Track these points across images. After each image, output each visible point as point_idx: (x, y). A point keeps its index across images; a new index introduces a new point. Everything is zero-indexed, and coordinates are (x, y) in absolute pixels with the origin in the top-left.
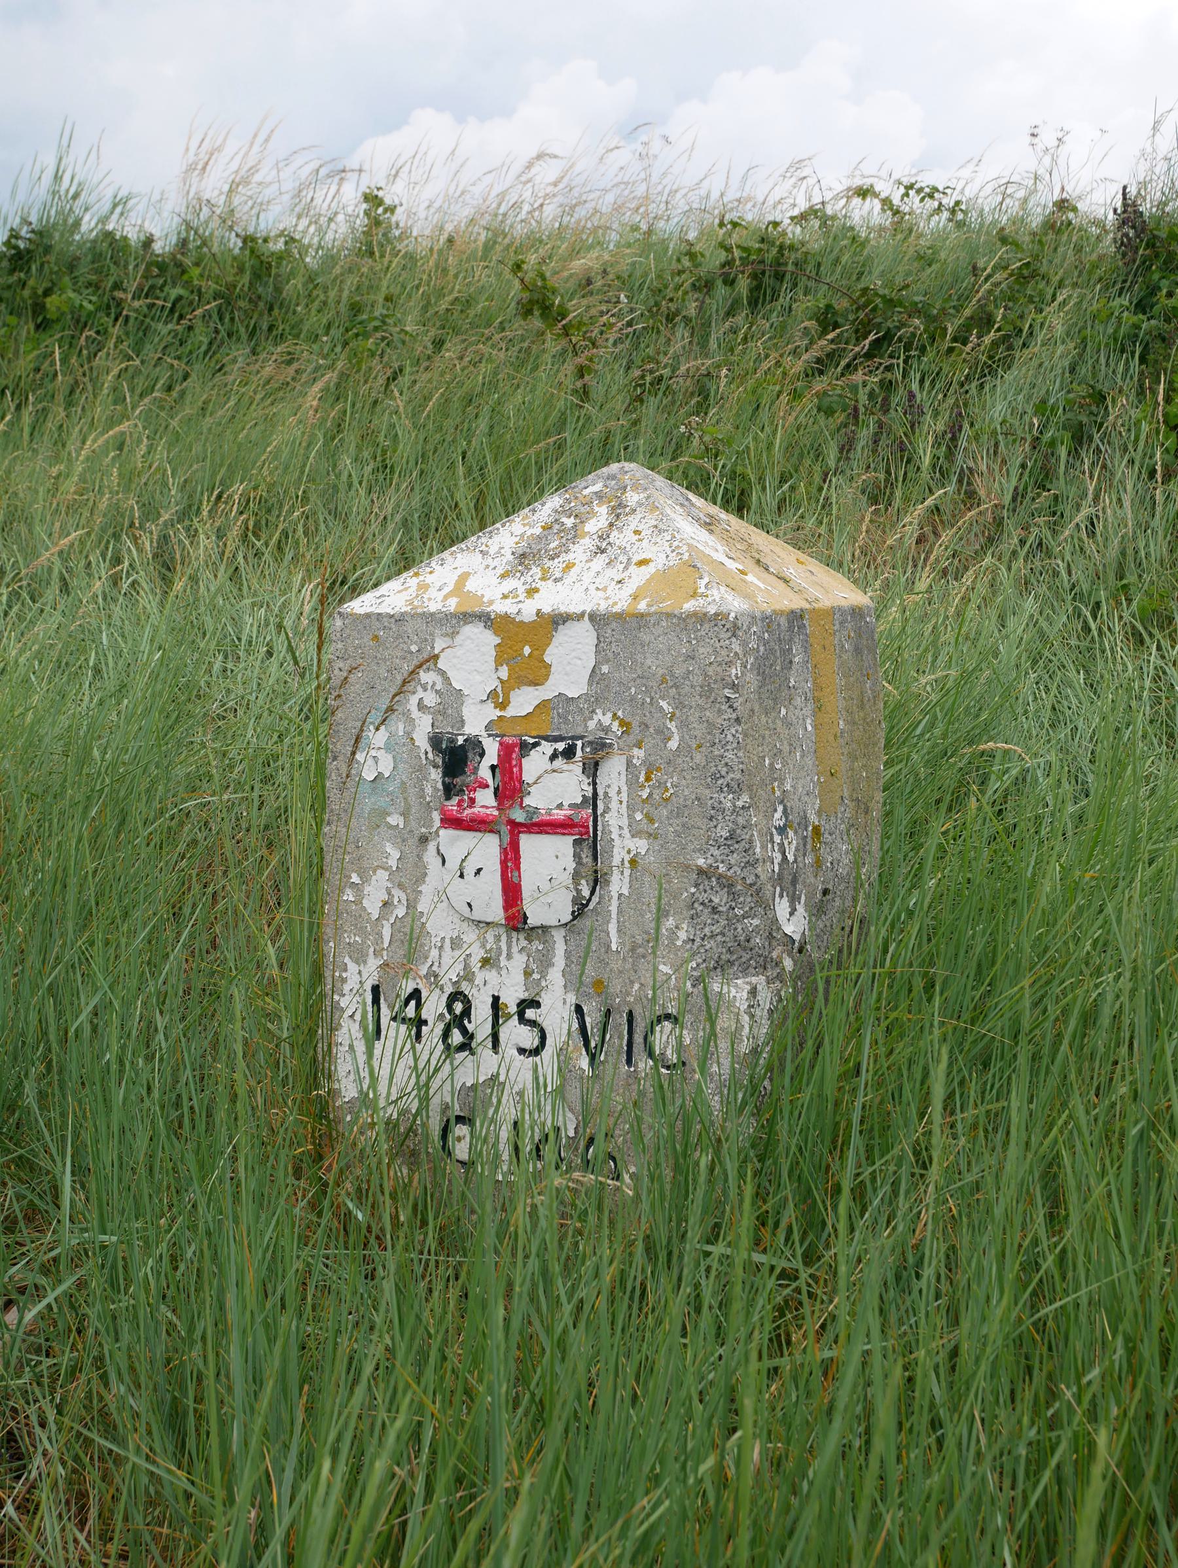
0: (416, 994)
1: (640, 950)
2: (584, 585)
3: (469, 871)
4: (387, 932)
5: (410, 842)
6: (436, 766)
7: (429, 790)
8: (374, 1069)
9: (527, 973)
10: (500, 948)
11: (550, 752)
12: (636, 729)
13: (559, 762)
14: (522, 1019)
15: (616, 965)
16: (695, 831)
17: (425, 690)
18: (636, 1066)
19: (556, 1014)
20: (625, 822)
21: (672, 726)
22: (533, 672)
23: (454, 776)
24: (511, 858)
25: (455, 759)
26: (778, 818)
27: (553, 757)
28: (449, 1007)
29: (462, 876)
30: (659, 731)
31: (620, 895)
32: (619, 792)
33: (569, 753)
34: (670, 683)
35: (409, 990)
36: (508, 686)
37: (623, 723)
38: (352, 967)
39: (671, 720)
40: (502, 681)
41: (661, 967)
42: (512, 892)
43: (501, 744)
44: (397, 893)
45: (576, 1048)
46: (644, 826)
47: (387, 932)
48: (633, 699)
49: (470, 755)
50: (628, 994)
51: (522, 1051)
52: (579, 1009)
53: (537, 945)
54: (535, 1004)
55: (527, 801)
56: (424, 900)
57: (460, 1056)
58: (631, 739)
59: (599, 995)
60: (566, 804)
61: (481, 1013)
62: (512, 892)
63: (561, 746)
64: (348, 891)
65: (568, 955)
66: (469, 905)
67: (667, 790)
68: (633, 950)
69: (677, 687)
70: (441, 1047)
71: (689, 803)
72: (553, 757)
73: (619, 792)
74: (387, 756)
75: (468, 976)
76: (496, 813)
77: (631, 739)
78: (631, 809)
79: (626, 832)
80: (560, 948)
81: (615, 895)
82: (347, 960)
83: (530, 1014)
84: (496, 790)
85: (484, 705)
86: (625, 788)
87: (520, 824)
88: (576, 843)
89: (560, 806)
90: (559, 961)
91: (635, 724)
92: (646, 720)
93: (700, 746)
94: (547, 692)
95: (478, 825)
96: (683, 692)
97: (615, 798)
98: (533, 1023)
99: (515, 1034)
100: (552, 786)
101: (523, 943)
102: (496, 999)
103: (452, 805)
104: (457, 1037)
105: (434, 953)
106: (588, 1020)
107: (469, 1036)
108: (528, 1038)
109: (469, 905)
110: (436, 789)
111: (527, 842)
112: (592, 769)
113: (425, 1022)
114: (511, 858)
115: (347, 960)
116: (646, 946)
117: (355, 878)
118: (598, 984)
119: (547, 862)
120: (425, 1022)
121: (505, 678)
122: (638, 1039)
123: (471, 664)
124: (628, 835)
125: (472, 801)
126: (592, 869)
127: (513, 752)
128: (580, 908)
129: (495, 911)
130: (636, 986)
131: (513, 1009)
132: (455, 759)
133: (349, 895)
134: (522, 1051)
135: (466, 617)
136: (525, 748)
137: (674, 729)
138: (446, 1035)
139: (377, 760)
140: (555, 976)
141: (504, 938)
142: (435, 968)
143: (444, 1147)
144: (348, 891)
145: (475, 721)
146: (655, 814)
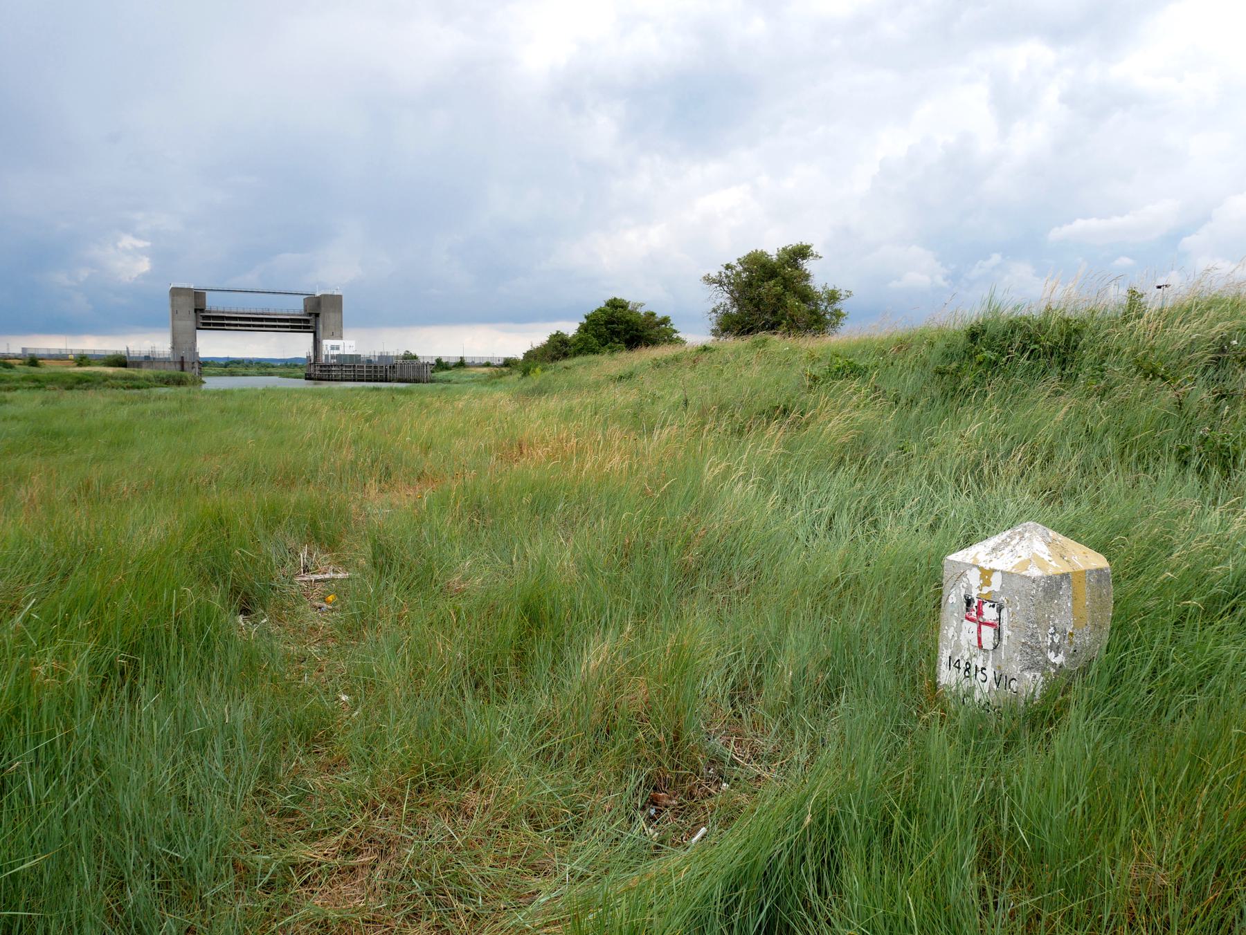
2: (1005, 562)
8: (947, 676)
19: (990, 673)
22: (987, 583)
24: (979, 630)
26: (1052, 630)
34: (1018, 592)
36: (982, 585)
42: (979, 639)
56: (958, 637)
61: (973, 670)
62: (979, 639)
74: (954, 598)
99: (979, 675)
100: (990, 614)
112: (999, 610)
114: (979, 630)
116: (1010, 660)
119: (988, 633)
123: (974, 577)
127: (981, 604)
128: (995, 647)
132: (969, 602)
135: (974, 566)
139: (953, 599)
140: (989, 663)
145: (974, 594)
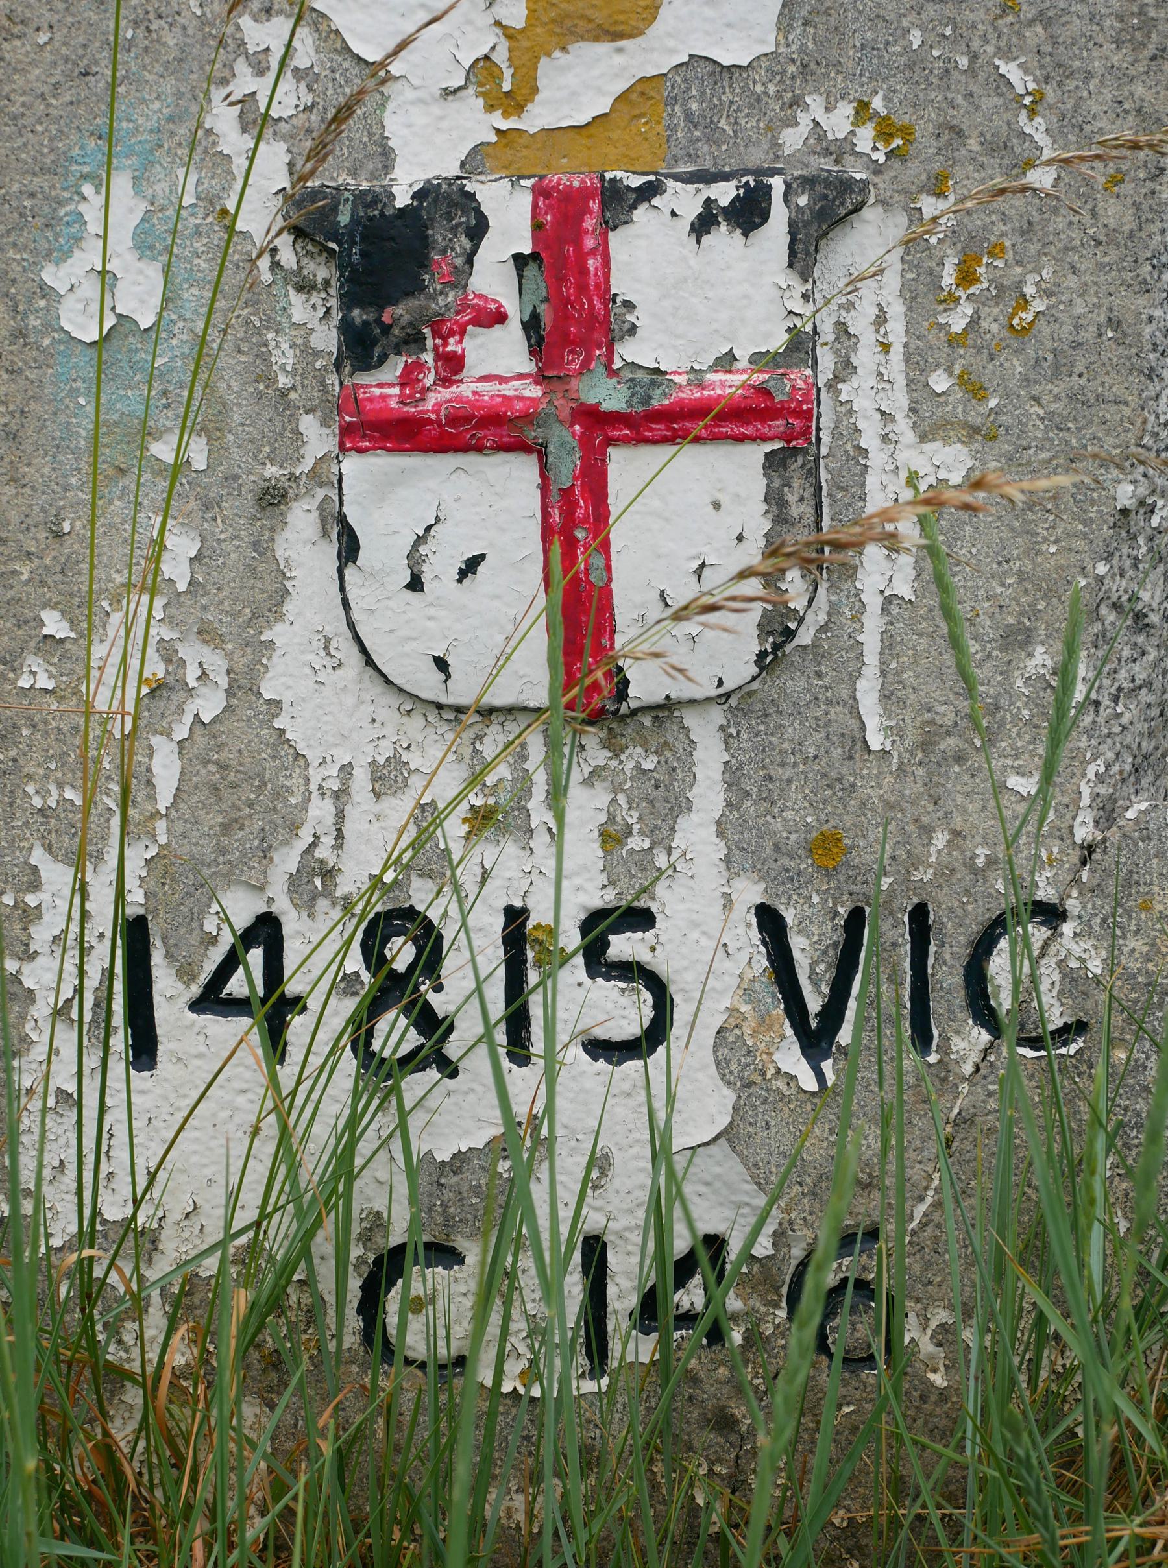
0: (266, 931)
1: (950, 743)
3: (441, 567)
4: (166, 768)
5: (229, 507)
6: (305, 287)
7: (284, 356)
9: (611, 838)
10: (526, 776)
11: (691, 208)
12: (926, 144)
13: (723, 238)
14: (596, 958)
15: (874, 788)
16: (1108, 412)
17: (260, 71)
18: (944, 1049)
19: (703, 936)
20: (899, 400)
21: (1037, 129)
23: (381, 301)
24: (575, 521)
25: (383, 261)
27: (703, 225)
28: (374, 957)
29: (415, 584)
30: (995, 147)
31: (888, 600)
32: (881, 319)
33: (748, 213)
35: (242, 919)
37: (885, 131)
38: (56, 877)
39: (1032, 112)
40: (509, 33)
41: (1013, 781)
42: (582, 616)
43: (540, 191)
44: (192, 653)
45: (764, 1022)
46: (958, 407)
47: (166, 768)
48: (914, 62)
49: (438, 235)
50: (915, 862)
51: (598, 1048)
52: (769, 921)
53: (639, 758)
54: (639, 918)
55: (628, 351)
57: (416, 1084)
58: (915, 171)
59: (829, 875)
60: (743, 355)
62: (582, 616)
63: (725, 193)
64: (33, 662)
65: (733, 776)
66: (441, 664)
67: (1023, 302)
68: (926, 744)
69: (1048, 23)
70: (349, 1063)
71: (1088, 335)
72: (703, 225)
73: (881, 319)
75: (423, 852)
76: (533, 391)
77: (915, 171)
78: (918, 363)
79: (903, 427)
80: (709, 758)
81: (874, 603)
82: (38, 856)
83: (623, 946)
84: (531, 326)
85: (453, 104)
86: (896, 310)
87: (615, 418)
88: (772, 462)
89: (726, 361)
90: (708, 794)
91: (923, 131)
92: (956, 116)
93: (1116, 180)
94: (658, 51)
95: (484, 430)
96: (1064, 35)
97: (868, 337)
98: (629, 971)
101: (597, 755)
102: (515, 917)
103: (383, 384)
104: (395, 1033)
105: (321, 811)
106: (798, 944)
107: (430, 1023)
108: (622, 1011)
109: (441, 664)
110: (307, 352)
111: (626, 468)
113: (297, 1004)
114: (575, 521)
115: (38, 856)
117: (54, 625)
118: (826, 848)
120: (297, 1004)
121: (519, 24)
122: (948, 975)
124: (909, 437)
125: (453, 364)
126: (811, 541)
129: (530, 677)
130: (940, 839)
131: (571, 938)
133: (37, 674)
134: (598, 1048)
136: (618, 203)
137: (1041, 138)
138: (360, 1034)
140: (698, 834)
141: (536, 749)
142: (324, 852)
143: (367, 1336)
144: (33, 662)
146: (988, 373)
